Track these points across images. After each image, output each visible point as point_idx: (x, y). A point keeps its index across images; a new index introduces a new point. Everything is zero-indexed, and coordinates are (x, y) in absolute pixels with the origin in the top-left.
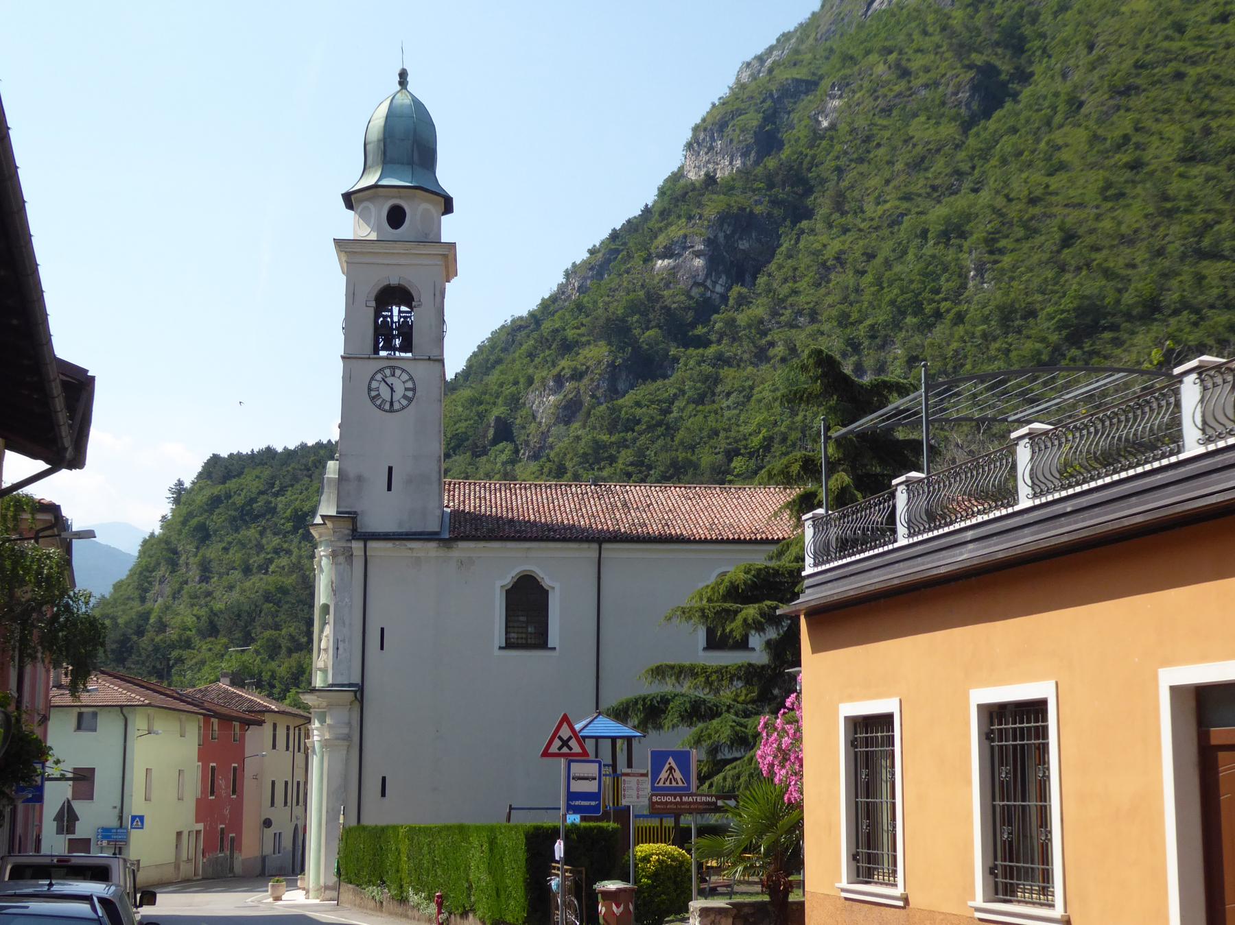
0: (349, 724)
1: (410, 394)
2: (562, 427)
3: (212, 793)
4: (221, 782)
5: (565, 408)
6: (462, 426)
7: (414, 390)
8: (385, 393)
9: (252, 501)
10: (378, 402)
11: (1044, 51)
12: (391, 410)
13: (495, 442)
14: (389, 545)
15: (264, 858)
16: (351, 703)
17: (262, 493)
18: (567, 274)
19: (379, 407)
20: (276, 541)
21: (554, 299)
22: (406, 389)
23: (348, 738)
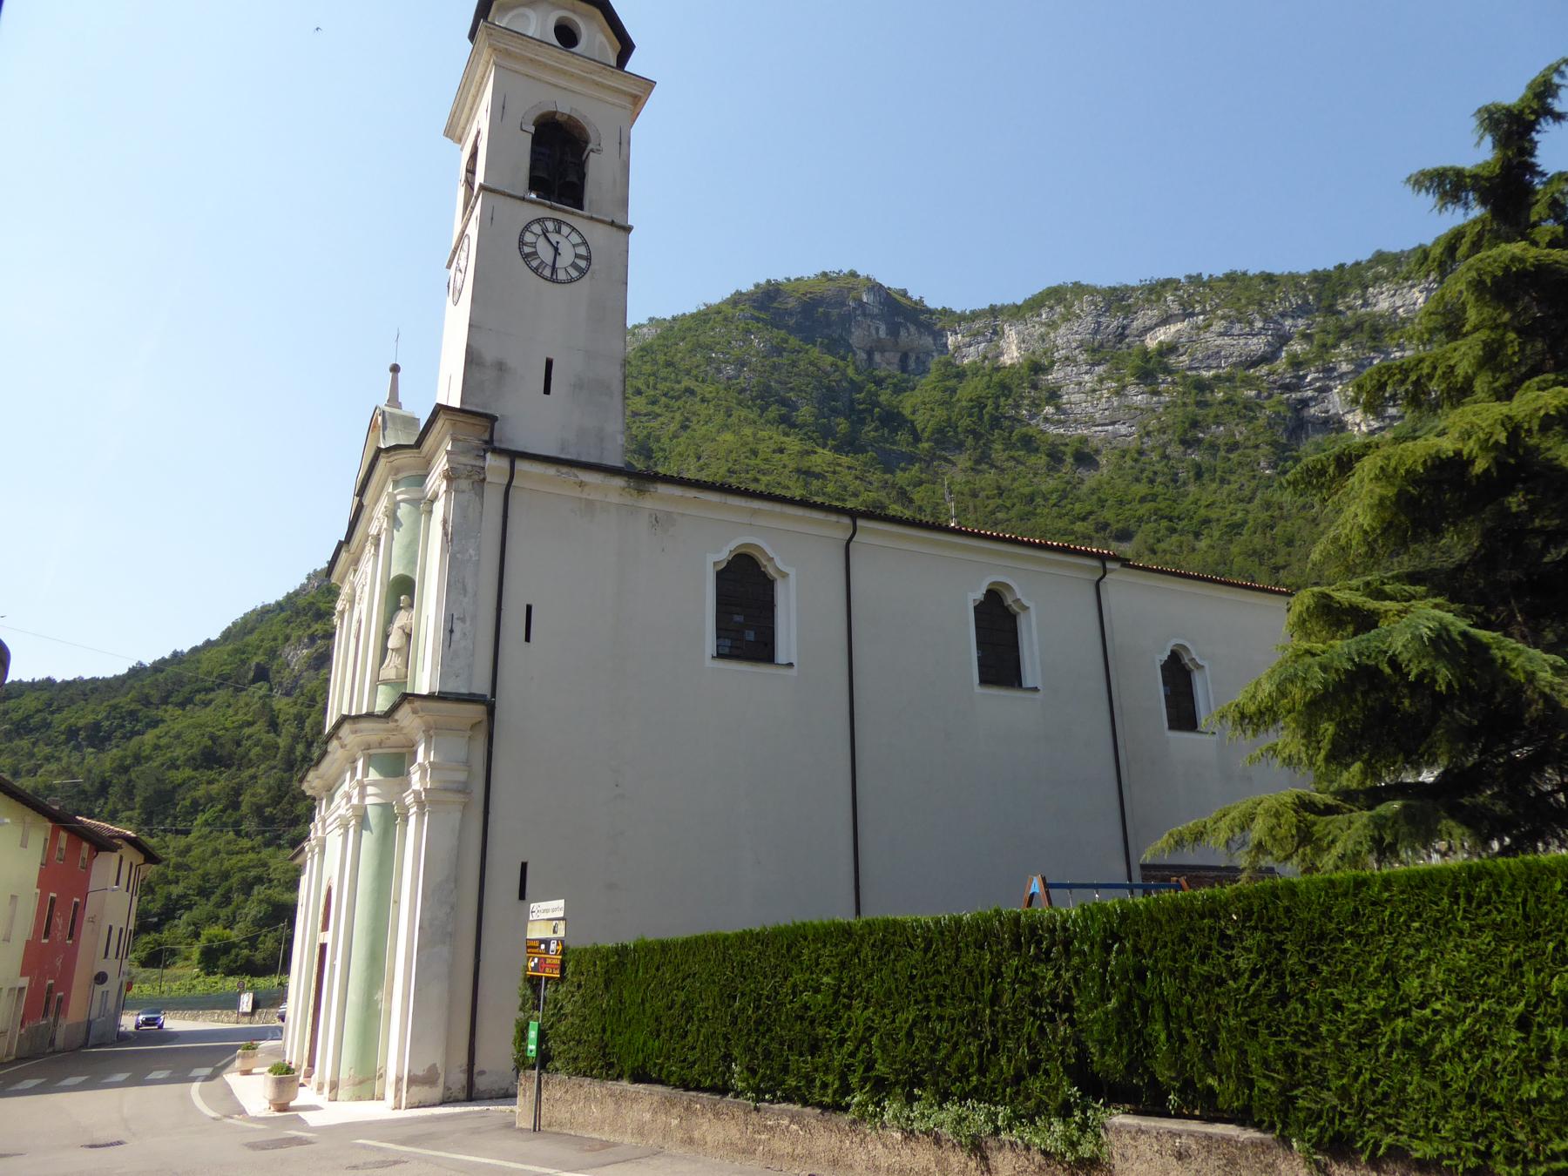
0: (467, 764)
1: (583, 264)
2: (312, 673)
3: (47, 935)
4: (58, 921)
6: (227, 669)
7: (588, 259)
8: (545, 253)
9: (29, 717)
12: (553, 279)
13: (254, 681)
14: (551, 471)
15: (89, 1023)
16: (473, 727)
17: (38, 711)
18: (309, 578)
19: (535, 270)
20: (48, 750)
21: (296, 593)
22: (577, 256)
23: (463, 789)
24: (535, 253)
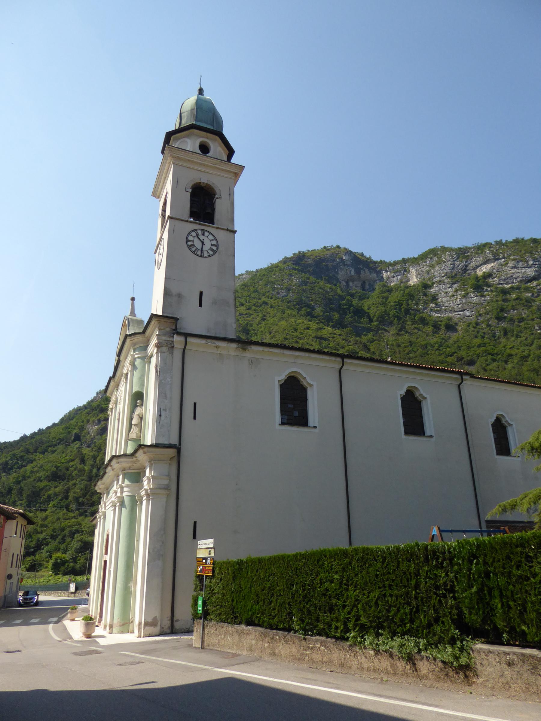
0: (169, 476)
1: (215, 248)
2: (99, 436)
5: (101, 430)
6: (62, 436)
7: (217, 246)
8: (198, 244)
10: (193, 249)
11: (255, 334)
13: (74, 441)
15: (5, 597)
16: (171, 459)
18: (97, 394)
19: (194, 252)
21: (92, 401)
22: (212, 245)
23: (167, 488)
24: (193, 245)
